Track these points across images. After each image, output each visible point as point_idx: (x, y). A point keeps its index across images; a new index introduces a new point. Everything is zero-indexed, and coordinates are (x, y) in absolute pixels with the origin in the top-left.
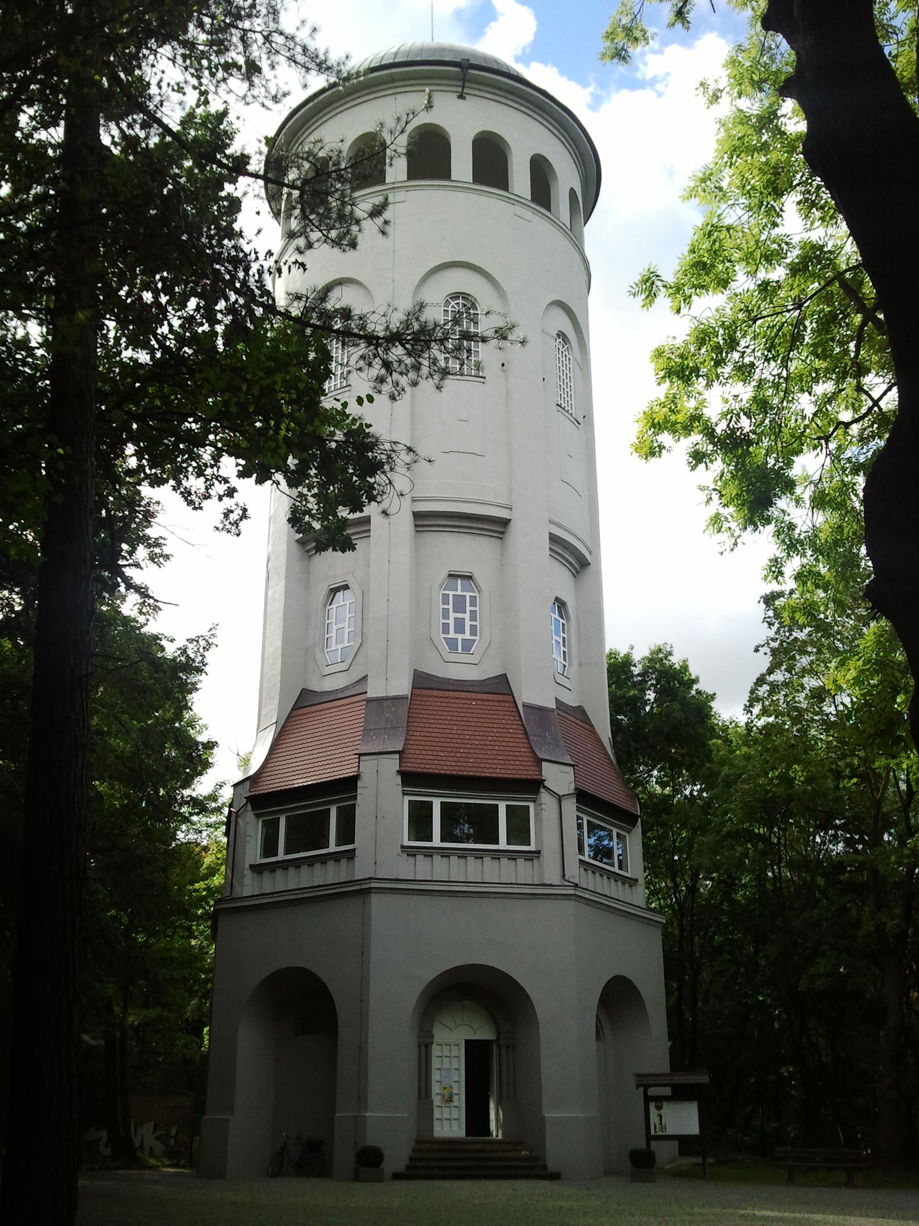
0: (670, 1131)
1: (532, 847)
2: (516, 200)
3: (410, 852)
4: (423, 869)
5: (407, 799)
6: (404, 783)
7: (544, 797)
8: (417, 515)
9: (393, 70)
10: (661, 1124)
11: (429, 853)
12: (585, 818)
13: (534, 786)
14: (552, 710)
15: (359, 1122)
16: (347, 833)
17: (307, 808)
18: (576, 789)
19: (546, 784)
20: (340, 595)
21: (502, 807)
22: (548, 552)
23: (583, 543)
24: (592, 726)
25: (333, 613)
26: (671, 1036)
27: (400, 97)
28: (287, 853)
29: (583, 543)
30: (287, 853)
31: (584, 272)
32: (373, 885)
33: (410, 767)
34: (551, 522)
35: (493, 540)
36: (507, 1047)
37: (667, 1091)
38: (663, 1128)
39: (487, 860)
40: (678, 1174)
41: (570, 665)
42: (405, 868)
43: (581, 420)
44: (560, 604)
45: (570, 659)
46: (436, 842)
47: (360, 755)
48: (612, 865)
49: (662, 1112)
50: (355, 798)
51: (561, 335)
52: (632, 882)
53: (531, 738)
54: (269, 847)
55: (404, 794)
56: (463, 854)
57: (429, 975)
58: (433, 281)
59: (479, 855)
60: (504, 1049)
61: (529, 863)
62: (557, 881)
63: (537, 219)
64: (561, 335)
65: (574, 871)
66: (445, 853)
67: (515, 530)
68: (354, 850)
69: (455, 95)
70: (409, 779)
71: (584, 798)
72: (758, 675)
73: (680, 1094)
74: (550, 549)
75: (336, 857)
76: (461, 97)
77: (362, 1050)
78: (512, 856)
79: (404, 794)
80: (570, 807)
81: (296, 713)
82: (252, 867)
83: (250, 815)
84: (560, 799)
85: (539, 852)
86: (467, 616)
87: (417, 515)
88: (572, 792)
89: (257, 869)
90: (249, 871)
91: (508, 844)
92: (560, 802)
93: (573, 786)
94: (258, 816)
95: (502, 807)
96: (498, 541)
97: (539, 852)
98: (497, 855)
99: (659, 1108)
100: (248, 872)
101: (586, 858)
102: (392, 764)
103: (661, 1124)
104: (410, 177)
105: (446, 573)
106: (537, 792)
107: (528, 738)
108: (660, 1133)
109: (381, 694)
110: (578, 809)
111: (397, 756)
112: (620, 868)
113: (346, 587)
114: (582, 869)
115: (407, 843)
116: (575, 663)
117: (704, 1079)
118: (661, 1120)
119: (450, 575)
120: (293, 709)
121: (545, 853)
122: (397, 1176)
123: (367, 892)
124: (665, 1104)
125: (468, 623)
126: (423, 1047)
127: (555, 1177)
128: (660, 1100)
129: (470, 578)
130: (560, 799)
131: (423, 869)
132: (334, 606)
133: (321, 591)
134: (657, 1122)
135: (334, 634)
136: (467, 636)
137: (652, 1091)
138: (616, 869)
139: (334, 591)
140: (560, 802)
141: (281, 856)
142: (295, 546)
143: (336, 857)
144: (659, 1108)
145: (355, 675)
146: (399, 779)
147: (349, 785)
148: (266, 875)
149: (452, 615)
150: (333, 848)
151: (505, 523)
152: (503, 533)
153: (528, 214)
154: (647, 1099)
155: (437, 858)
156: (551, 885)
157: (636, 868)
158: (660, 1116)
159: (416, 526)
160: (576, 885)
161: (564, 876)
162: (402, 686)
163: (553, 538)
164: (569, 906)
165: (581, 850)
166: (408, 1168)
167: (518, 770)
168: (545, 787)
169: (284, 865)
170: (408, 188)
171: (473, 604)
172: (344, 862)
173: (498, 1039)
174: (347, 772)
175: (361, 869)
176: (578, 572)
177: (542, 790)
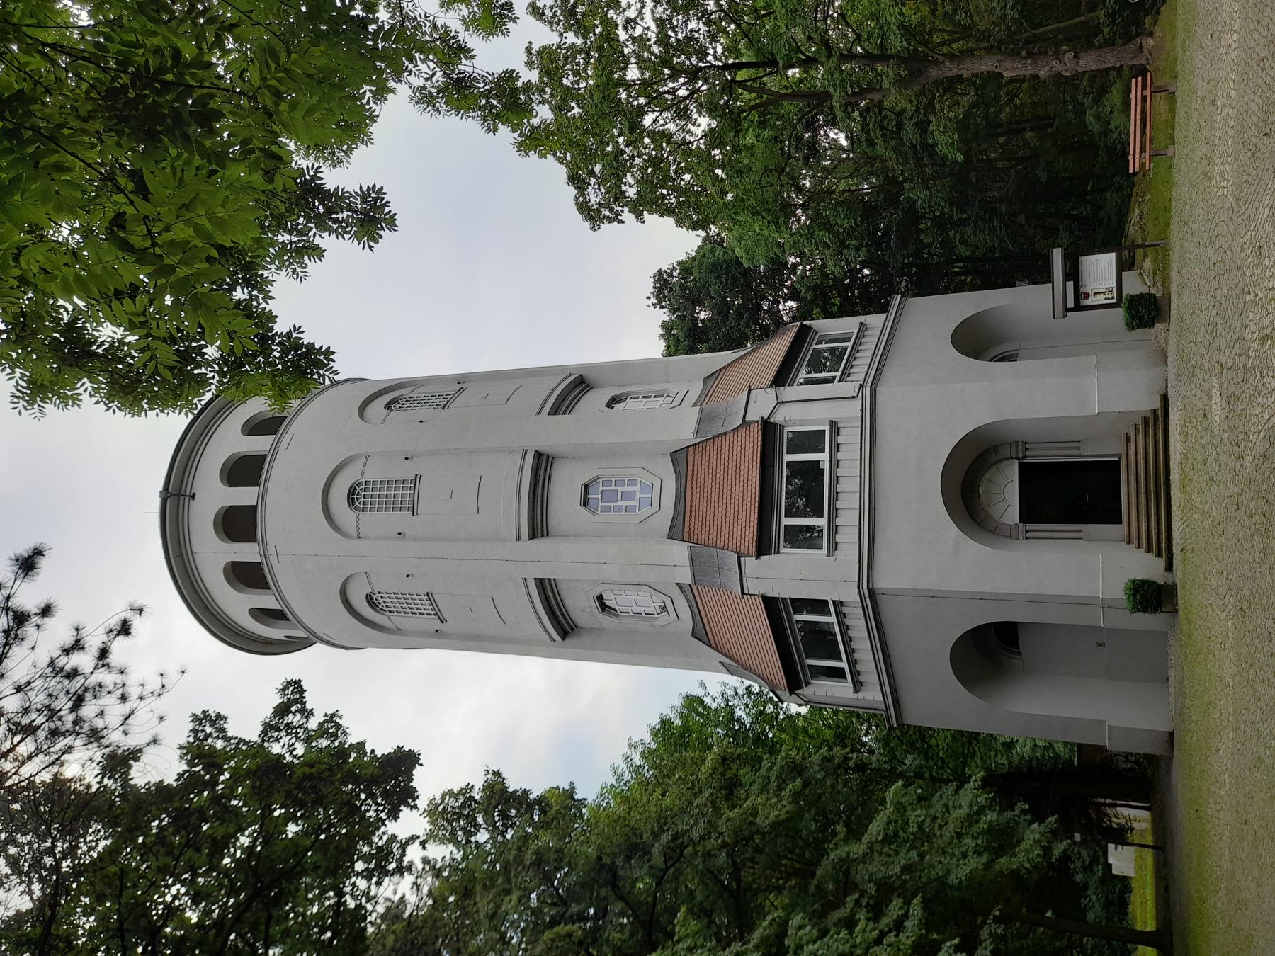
0: (1112, 283)
1: (827, 428)
2: (275, 448)
3: (833, 547)
4: (849, 536)
5: (782, 550)
6: (769, 553)
7: (778, 418)
8: (533, 536)
9: (171, 557)
10: (1104, 293)
11: (834, 529)
12: (803, 375)
13: (769, 429)
14: (701, 411)
15: (1108, 605)
16: (818, 606)
17: (797, 640)
18: (771, 386)
19: (765, 417)
20: (608, 603)
21: (789, 458)
22: (566, 416)
23: (564, 380)
24: (721, 369)
25: (623, 609)
26: (1010, 284)
27: (194, 550)
28: (840, 659)
29: (564, 380)
30: (840, 659)
31: (345, 385)
32: (865, 586)
33: (752, 547)
34: (539, 414)
35: (554, 466)
36: (1026, 449)
37: (1070, 285)
38: (1109, 290)
39: (839, 472)
40: (1162, 271)
41: (666, 391)
42: (849, 553)
43: (460, 386)
44: (613, 402)
45: (662, 391)
46: (822, 522)
47: (743, 593)
48: (846, 348)
49: (1091, 293)
50: (784, 599)
51: (388, 406)
52: (863, 328)
53: (725, 430)
54: (837, 674)
55: (778, 553)
56: (835, 496)
57: (952, 530)
58: (340, 521)
59: (835, 480)
60: (1027, 453)
61: (842, 431)
62: (858, 403)
63: (292, 430)
64: (388, 406)
65: (850, 388)
66: (834, 513)
67: (546, 445)
68: (834, 601)
69: (192, 502)
70: (763, 548)
71: (782, 377)
72: (575, 208)
73: (1073, 273)
74: (564, 414)
75: (841, 617)
76: (193, 497)
77: (1032, 600)
78: (835, 447)
79: (778, 553)
80: (789, 392)
81: (713, 645)
82: (856, 691)
83: (807, 691)
84: (780, 403)
85: (831, 422)
86: (620, 489)
87: (533, 536)
88: (773, 391)
89: (858, 686)
90: (860, 694)
91: (823, 451)
92: (783, 402)
93: (769, 390)
94: (808, 684)
95: (789, 458)
96: (555, 461)
97: (831, 422)
98: (834, 462)
99: (1087, 296)
100: (861, 695)
101: (838, 374)
102: (750, 564)
103: (1104, 293)
104: (255, 541)
105: (582, 509)
106: (775, 424)
107: (726, 433)
108: (1114, 294)
109: (688, 570)
110: (791, 384)
111: (742, 559)
112: (848, 339)
113: (600, 598)
114: (849, 379)
115: (825, 551)
116: (665, 386)
117: (1057, 255)
118: (1099, 293)
119: (585, 505)
120: (710, 646)
121: (834, 417)
122: (1169, 568)
123: (872, 592)
124: (1083, 290)
125: (626, 488)
126: (1028, 535)
127: (1165, 400)
128: (1079, 296)
129: (586, 488)
130: (780, 403)
131: (849, 536)
132: (617, 608)
133: (605, 619)
134: (1102, 297)
135: (642, 609)
136: (637, 489)
137: (1071, 304)
138: (850, 344)
139: (604, 607)
140: (783, 402)
141: (843, 664)
142: (567, 641)
143: (841, 617)
144: (1087, 296)
145: (676, 593)
146: (764, 558)
147: (771, 604)
148: (862, 678)
149: (619, 503)
150: (832, 619)
151: (539, 455)
152: (548, 457)
153: (287, 438)
154: (1078, 307)
155: (839, 521)
156: (862, 410)
157: (848, 325)
158: (1095, 294)
159: (542, 536)
160: (861, 386)
161: (853, 397)
162: (680, 551)
163: (555, 411)
164: (881, 390)
165: (832, 380)
166: (1159, 555)
167: (753, 441)
168: (769, 418)
169: (852, 663)
170: (265, 543)
171: (608, 483)
172: (845, 610)
173: (1018, 458)
174: (760, 604)
175: (850, 595)
176: (588, 386)
177: (772, 420)
